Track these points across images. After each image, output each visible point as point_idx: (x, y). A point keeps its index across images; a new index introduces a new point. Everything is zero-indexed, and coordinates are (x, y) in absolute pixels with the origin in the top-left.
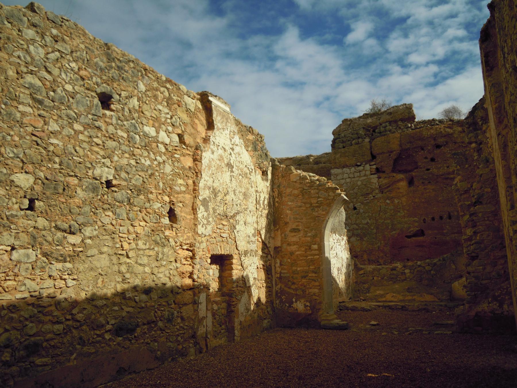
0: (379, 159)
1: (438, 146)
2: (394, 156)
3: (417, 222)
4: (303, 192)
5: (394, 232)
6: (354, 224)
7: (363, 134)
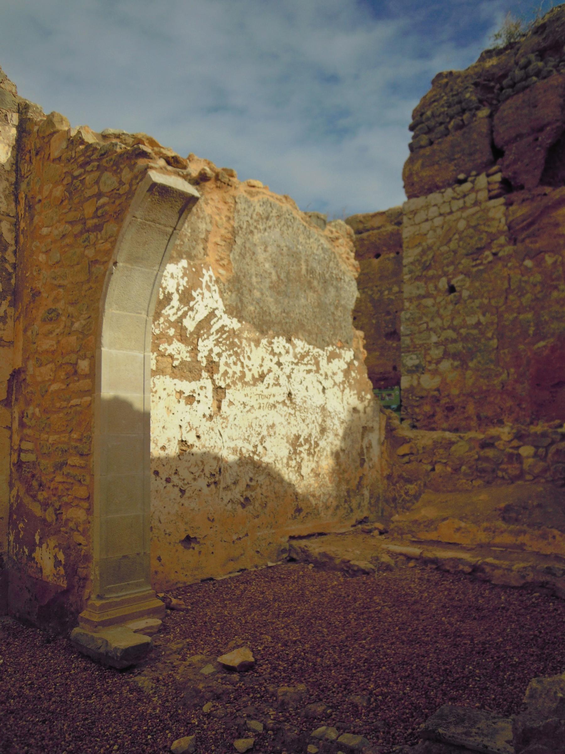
0: (509, 157)
5: (542, 344)
6: (449, 327)
7: (474, 98)
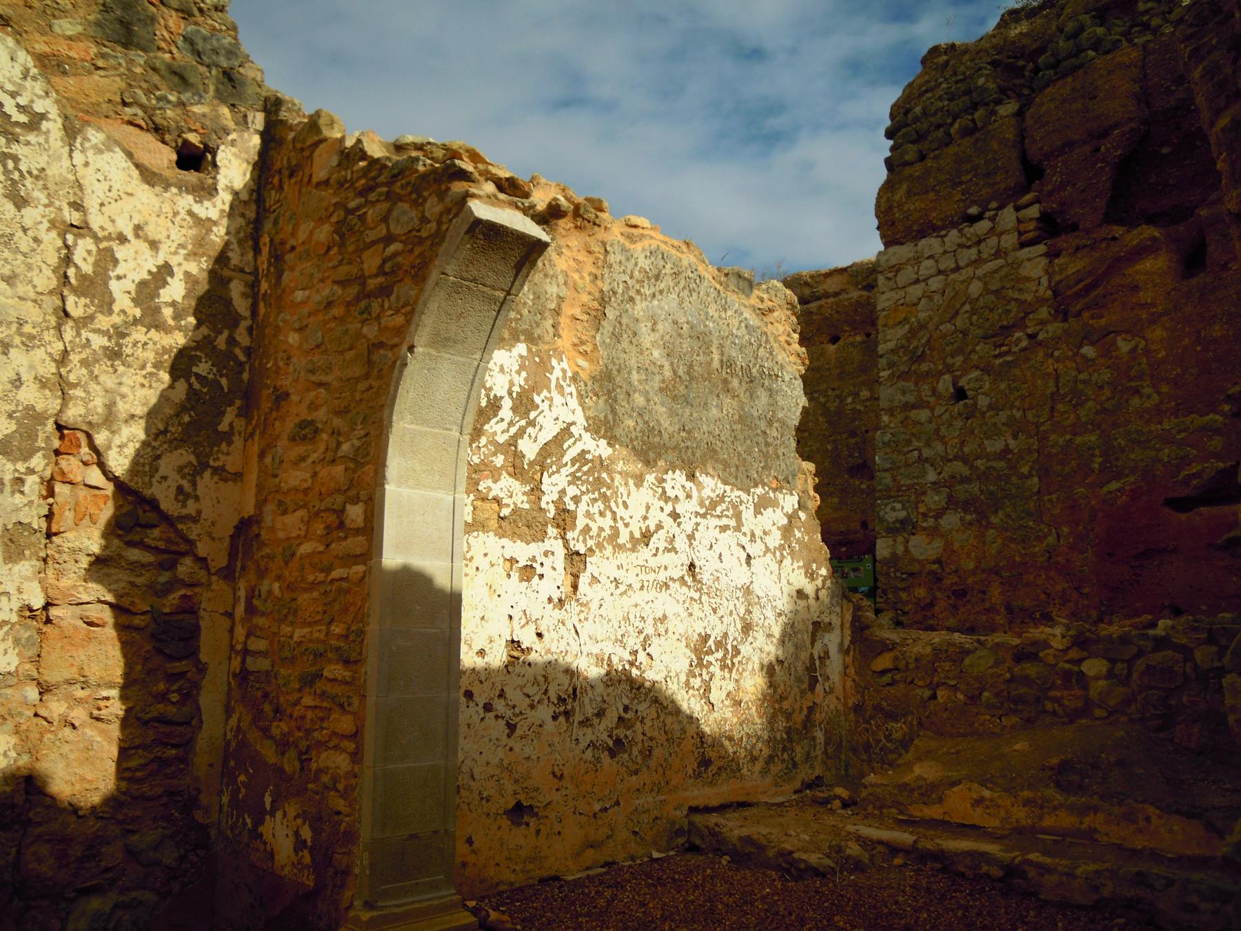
3: (1217, 431)
5: (1114, 485)
6: (956, 458)
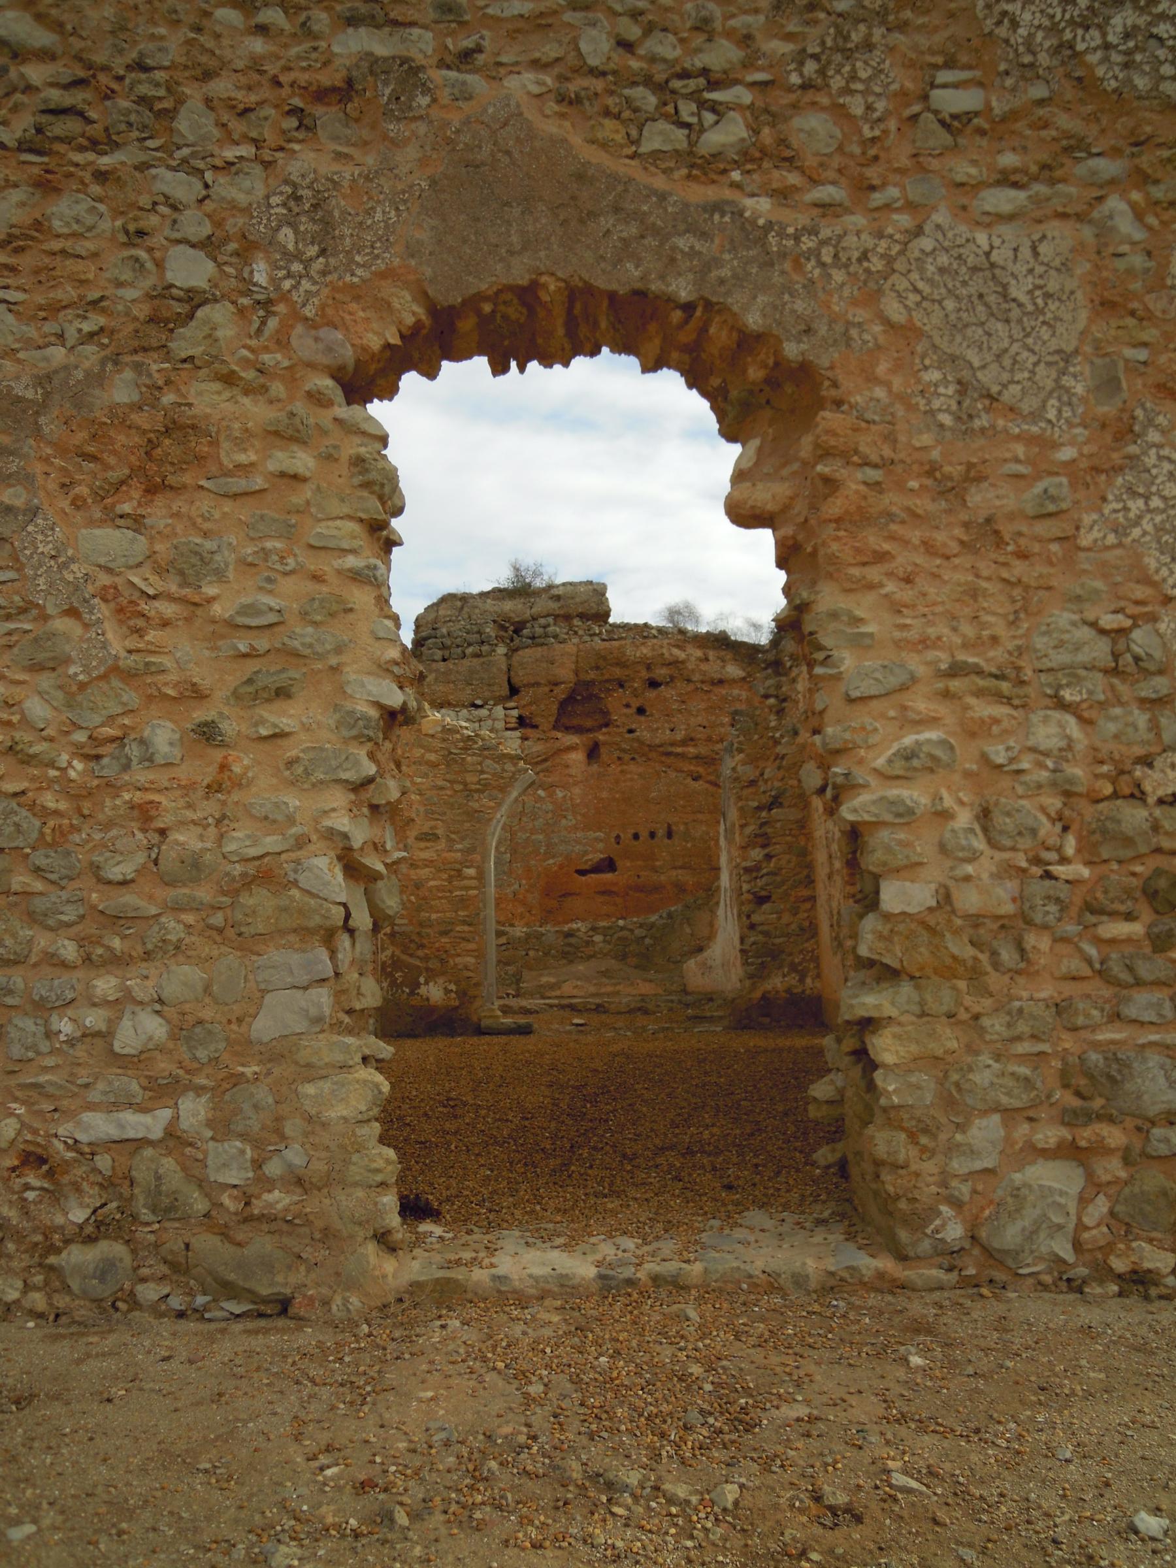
0: (526, 697)
1: (654, 684)
2: (561, 692)
4: (449, 759)
5: (551, 861)
